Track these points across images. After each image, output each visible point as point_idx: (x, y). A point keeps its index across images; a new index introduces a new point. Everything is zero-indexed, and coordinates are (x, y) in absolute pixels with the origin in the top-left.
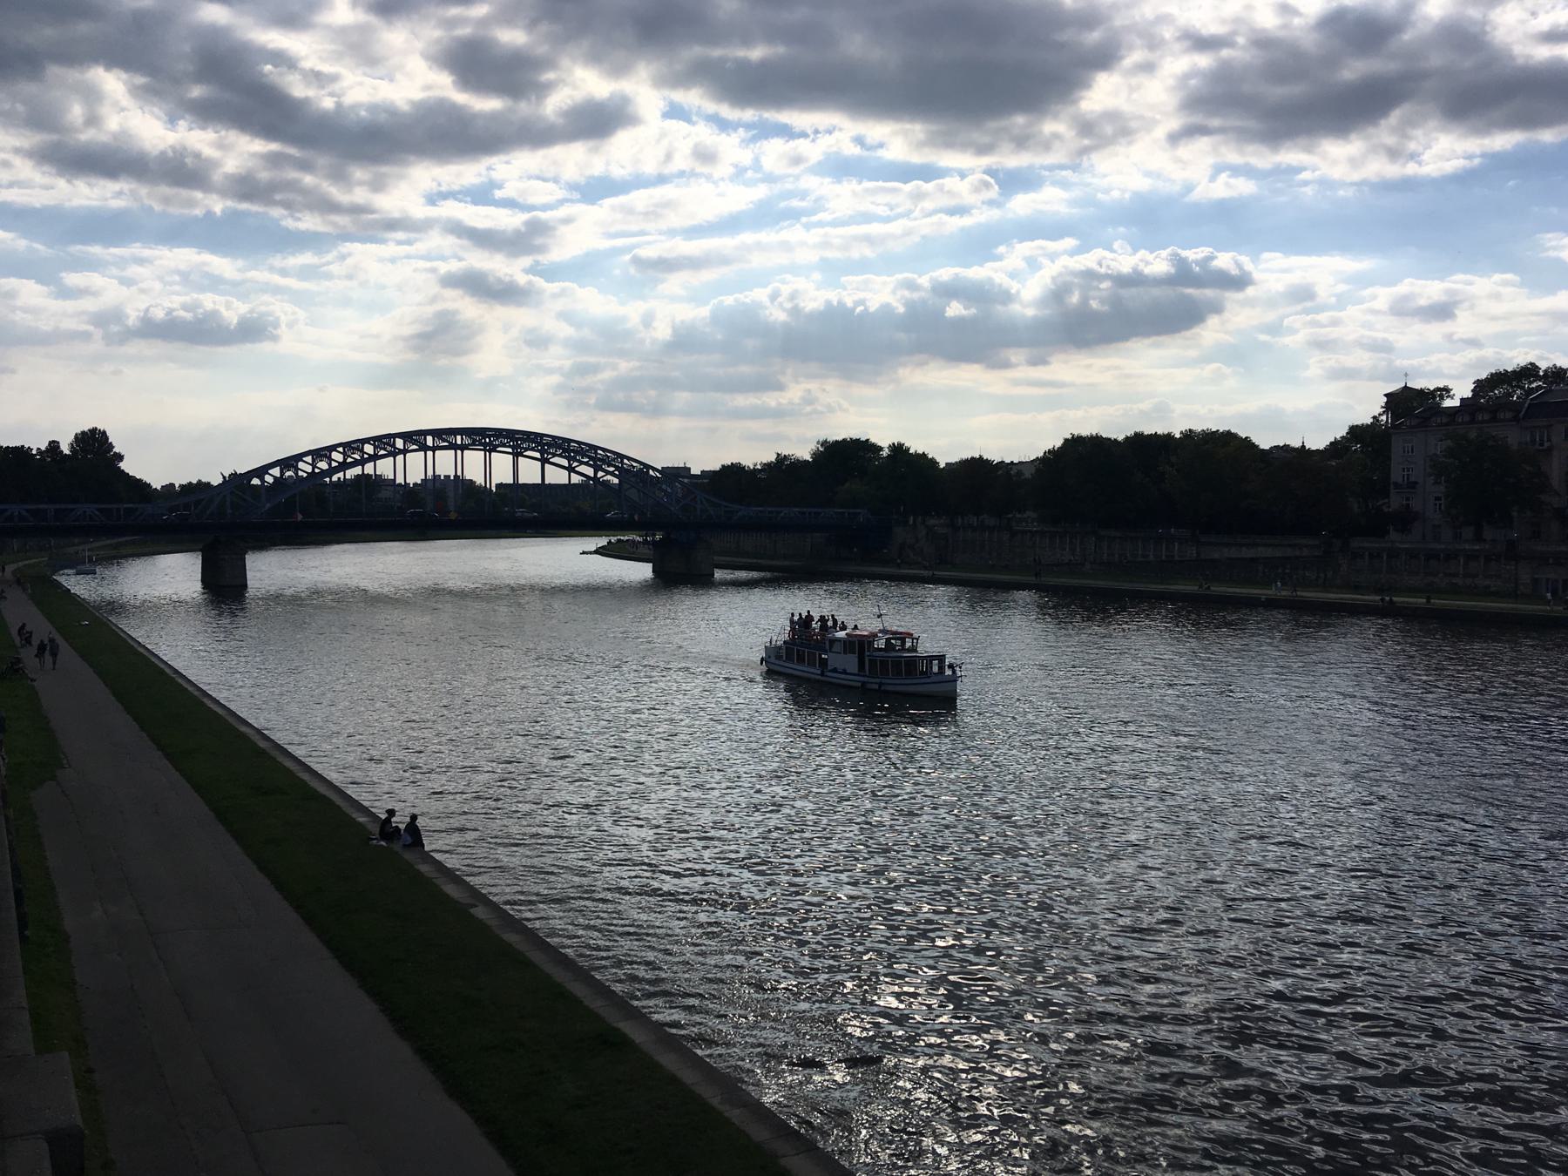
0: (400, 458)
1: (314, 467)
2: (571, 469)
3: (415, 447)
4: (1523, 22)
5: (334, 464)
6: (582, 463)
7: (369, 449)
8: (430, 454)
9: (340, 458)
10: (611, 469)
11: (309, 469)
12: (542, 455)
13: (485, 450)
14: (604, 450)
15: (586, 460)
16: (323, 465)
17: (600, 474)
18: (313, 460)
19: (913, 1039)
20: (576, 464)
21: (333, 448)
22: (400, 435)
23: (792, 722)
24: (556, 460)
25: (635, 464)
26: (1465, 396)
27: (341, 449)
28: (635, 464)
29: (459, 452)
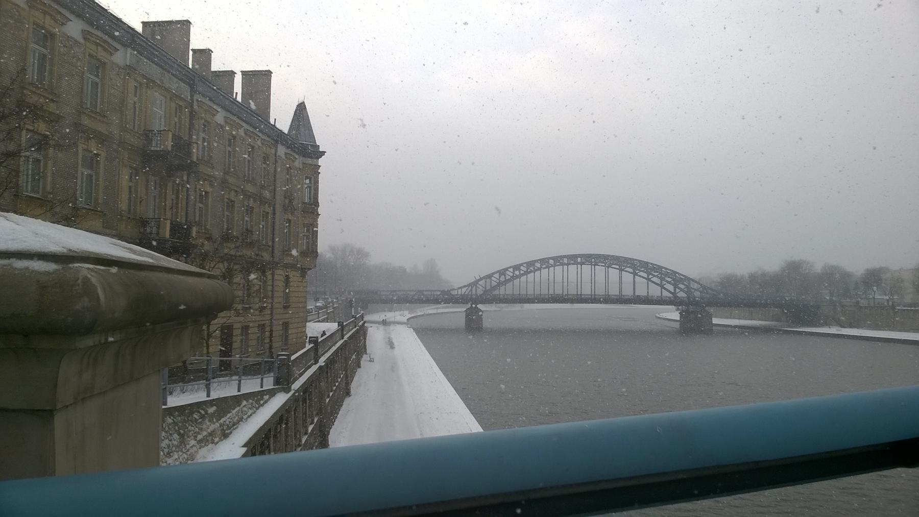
0: (551, 269)
1: (514, 274)
2: (662, 287)
3: (558, 264)
4: (24, 18)
5: (522, 272)
6: (654, 276)
7: (538, 265)
8: (565, 267)
9: (525, 269)
10: (656, 274)
11: (512, 275)
12: (634, 270)
13: (591, 265)
14: (666, 269)
15: (643, 269)
16: (517, 273)
17: (650, 276)
18: (514, 271)
19: (391, 293)
20: (637, 272)
21: (521, 265)
22: (552, 258)
23: (102, 54)
24: (627, 269)
25: (682, 277)
26: (193, 31)
27: (525, 265)
28: (682, 277)
29: (579, 266)
